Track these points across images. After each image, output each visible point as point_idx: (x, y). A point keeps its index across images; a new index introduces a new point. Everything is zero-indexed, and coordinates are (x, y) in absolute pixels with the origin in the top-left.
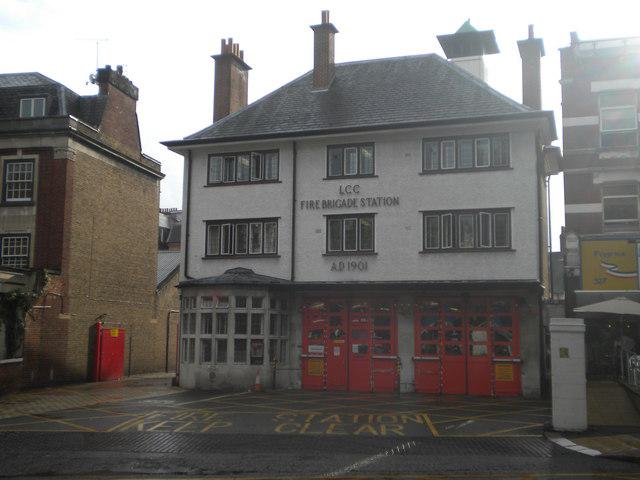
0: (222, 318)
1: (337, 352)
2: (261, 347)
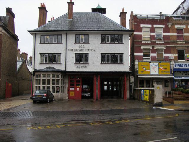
0: (49, 81)
1: (78, 90)
2: (59, 88)
